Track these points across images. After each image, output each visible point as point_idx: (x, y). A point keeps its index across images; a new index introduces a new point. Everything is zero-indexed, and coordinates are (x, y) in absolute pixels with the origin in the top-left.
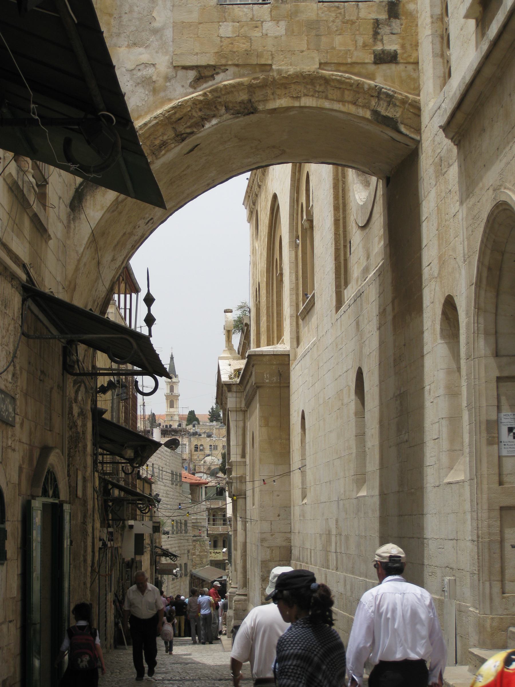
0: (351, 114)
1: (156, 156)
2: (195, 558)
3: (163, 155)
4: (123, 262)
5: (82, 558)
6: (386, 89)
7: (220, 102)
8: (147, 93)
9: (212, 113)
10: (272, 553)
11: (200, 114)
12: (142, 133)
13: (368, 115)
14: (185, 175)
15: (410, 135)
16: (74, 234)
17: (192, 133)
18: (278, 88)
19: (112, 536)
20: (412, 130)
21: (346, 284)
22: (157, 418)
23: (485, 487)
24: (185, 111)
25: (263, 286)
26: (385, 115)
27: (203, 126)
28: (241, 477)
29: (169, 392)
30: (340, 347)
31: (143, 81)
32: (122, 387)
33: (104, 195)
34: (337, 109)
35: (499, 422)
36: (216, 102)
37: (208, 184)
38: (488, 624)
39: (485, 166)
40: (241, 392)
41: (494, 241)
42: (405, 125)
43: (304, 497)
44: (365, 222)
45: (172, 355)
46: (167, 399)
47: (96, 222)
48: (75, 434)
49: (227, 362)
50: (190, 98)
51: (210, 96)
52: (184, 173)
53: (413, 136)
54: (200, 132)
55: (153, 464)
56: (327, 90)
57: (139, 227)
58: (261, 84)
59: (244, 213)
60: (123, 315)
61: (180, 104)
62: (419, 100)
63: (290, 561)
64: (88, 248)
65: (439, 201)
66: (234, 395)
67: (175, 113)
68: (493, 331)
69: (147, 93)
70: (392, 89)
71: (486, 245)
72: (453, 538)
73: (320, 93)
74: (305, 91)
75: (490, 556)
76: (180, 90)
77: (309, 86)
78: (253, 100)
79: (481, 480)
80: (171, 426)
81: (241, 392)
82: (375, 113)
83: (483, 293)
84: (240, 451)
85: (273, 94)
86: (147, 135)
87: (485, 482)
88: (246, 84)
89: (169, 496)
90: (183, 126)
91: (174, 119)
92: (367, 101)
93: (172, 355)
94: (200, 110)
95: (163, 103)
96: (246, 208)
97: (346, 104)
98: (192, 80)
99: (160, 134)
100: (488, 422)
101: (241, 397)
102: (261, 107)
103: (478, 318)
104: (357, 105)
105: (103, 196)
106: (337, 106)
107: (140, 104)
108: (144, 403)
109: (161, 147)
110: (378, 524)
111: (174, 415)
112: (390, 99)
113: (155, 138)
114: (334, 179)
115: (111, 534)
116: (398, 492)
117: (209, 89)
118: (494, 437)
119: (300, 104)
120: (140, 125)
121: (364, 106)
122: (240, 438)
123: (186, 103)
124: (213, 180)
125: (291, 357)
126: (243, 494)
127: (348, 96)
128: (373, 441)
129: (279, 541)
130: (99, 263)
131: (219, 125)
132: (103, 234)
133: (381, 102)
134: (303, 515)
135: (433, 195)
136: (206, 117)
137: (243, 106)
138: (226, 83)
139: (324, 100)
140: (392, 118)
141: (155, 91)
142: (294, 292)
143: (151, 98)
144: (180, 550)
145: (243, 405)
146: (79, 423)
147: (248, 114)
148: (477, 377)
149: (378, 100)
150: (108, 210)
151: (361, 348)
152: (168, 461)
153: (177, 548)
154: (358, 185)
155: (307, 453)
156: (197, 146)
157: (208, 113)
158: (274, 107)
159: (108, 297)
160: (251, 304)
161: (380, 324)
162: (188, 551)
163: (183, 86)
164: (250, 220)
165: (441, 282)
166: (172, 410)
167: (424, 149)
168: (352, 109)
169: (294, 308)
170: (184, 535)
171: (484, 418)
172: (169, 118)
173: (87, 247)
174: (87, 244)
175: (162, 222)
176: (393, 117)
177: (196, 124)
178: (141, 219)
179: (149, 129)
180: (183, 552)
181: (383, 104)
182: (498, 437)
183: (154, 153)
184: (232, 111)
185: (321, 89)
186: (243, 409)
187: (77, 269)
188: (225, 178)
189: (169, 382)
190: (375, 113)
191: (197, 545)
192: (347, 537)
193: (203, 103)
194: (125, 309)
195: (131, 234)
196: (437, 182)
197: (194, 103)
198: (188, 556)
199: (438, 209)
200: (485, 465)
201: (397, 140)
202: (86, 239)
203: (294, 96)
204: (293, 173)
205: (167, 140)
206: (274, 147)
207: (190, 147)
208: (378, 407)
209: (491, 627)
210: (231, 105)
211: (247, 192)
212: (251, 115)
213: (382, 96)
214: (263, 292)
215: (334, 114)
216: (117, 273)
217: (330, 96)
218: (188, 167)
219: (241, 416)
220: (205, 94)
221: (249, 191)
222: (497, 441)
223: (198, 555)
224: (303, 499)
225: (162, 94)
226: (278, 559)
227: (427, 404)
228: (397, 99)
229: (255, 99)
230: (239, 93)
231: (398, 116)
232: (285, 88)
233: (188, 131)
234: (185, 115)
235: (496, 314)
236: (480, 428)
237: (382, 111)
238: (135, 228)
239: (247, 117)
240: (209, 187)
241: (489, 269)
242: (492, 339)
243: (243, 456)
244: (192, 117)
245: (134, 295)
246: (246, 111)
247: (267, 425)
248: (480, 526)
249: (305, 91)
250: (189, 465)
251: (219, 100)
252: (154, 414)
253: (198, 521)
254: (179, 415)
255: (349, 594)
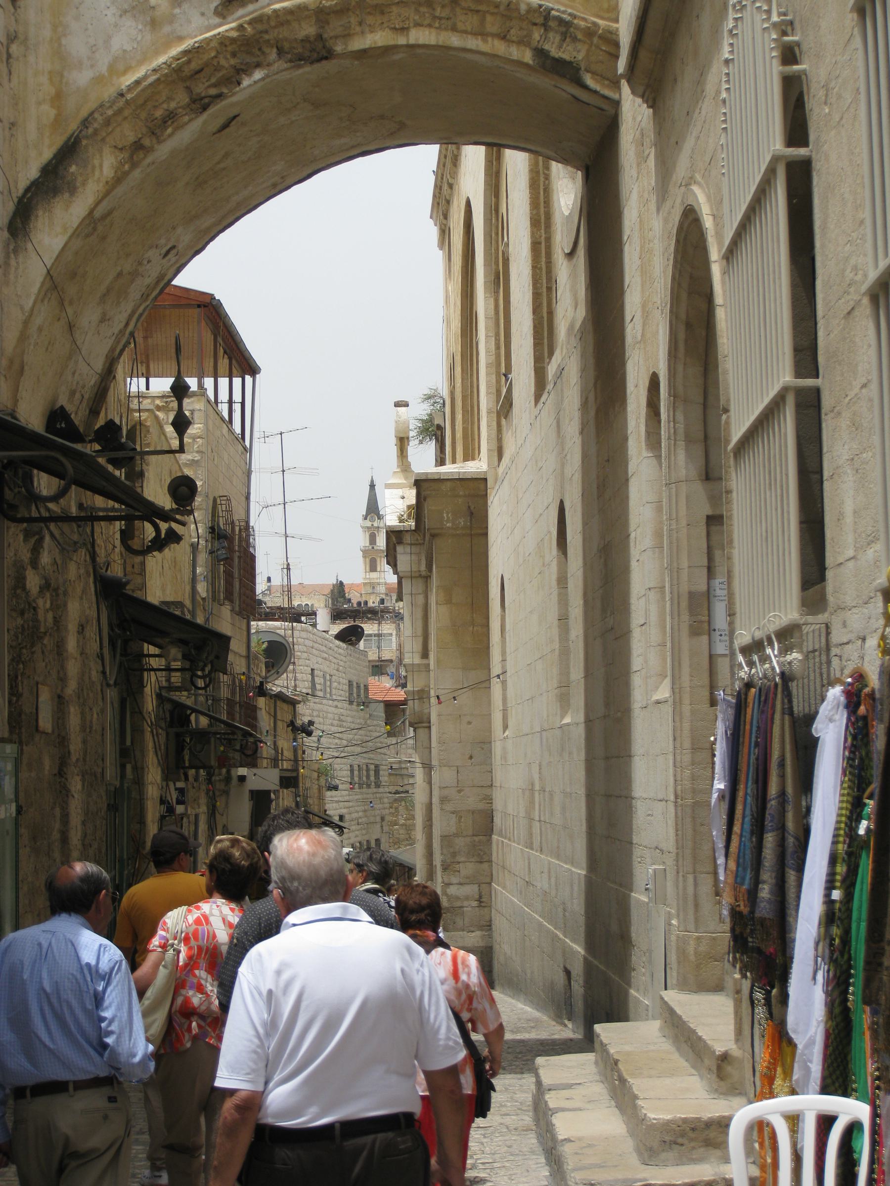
0: (498, 56)
1: (157, 138)
2: (397, 830)
3: (170, 136)
4: (127, 324)
5: (56, 835)
6: (558, 10)
7: (268, 41)
8: (140, 27)
9: (255, 60)
10: (460, 821)
11: (233, 62)
12: (132, 99)
13: (528, 57)
14: (224, 169)
15: (602, 92)
16: (16, 277)
17: (220, 96)
18: (370, 13)
19: (183, 796)
20: (606, 82)
21: (551, 353)
22: (346, 590)
23: (686, 709)
24: (206, 57)
25: (458, 358)
26: (557, 56)
27: (239, 84)
28: (421, 691)
29: (368, 544)
30: (540, 465)
31: (133, 8)
32: (218, 539)
33: (67, 207)
34: (474, 47)
35: (711, 596)
36: (261, 40)
37: (275, 185)
38: (691, 949)
39: (677, 143)
40: (420, 544)
41: (691, 277)
42: (594, 73)
43: (505, 727)
44: (571, 244)
45: (372, 481)
46: (364, 557)
47: (55, 256)
48: (31, 623)
49: (400, 492)
50: (215, 35)
51: (249, 29)
52: (222, 165)
53: (607, 92)
54: (234, 94)
55: (312, 670)
56: (455, 15)
57: (149, 262)
58: (338, 8)
59: (433, 231)
60: (226, 415)
61: (196, 45)
62: (617, 29)
63: (491, 836)
64: (42, 301)
65: (642, 206)
66: (408, 549)
67: (189, 62)
68: (701, 436)
69: (140, 27)
70: (570, 11)
71: (679, 284)
72: (662, 798)
73: (443, 21)
74: (417, 17)
75: (694, 831)
76: (197, 21)
77: (423, 9)
78: (325, 36)
79: (680, 698)
80: (366, 603)
81: (420, 544)
82: (540, 53)
83: (680, 368)
84: (418, 647)
85: (360, 24)
86: (140, 102)
87: (686, 701)
88: (312, 7)
89: (344, 724)
90: (203, 83)
91: (187, 71)
92: (525, 33)
93: (372, 481)
94: (234, 55)
95: (168, 45)
96: (436, 225)
97: (490, 39)
98: (218, 3)
99: (164, 98)
100: (691, 595)
101: (420, 553)
102: (339, 48)
103: (674, 411)
104: (509, 41)
105: (66, 210)
106: (473, 43)
107: (128, 47)
108: (288, 565)
109: (165, 122)
110: (584, 773)
111: (379, 584)
112: (566, 28)
113: (155, 107)
114: (531, 171)
115: (181, 791)
116: (605, 717)
117: (247, 19)
118: (701, 622)
119: (408, 40)
120: (128, 83)
121: (520, 42)
122: (419, 624)
123: (208, 44)
124: (282, 178)
125: (490, 483)
126: (425, 720)
127: (492, 24)
128: (577, 630)
129: (472, 801)
130: (71, 327)
131: (268, 80)
132: (73, 275)
133: (551, 35)
134: (504, 757)
135: (634, 196)
136: (243, 67)
137: (308, 45)
138: (277, 6)
139: (450, 33)
140: (570, 63)
141: (154, 24)
142: (494, 370)
143: (148, 37)
144: (366, 816)
145: (423, 567)
146: (43, 604)
147: (320, 60)
148: (674, 516)
149: (546, 30)
150: (75, 234)
151: (563, 465)
152: (342, 663)
153: (361, 814)
154: (565, 180)
155: (508, 650)
156: (235, 117)
157: (248, 60)
158: (362, 47)
159: (103, 384)
160: (445, 393)
161: (582, 423)
162: (383, 819)
163: (203, 14)
164: (441, 245)
165: (645, 349)
166: (374, 575)
167: (624, 118)
168: (499, 47)
169: (494, 397)
170: (375, 790)
171: (685, 588)
172: (179, 70)
173: (42, 297)
174: (39, 291)
175: (198, 252)
176: (572, 60)
177: (227, 79)
178: (151, 247)
179: (143, 90)
180: (372, 819)
181: (554, 38)
182: (709, 622)
183: (153, 133)
184: (289, 56)
185: (446, 13)
186: (424, 573)
187: (23, 337)
188: (305, 174)
189: (368, 528)
190: (540, 53)
191: (400, 808)
192: (551, 794)
193: (239, 43)
194: (231, 402)
195: (135, 275)
196: (638, 173)
197: (221, 44)
198: (382, 827)
199: (641, 221)
200: (686, 670)
201: (585, 100)
202: (38, 285)
203: (397, 26)
204: (441, 164)
205: (176, 109)
206: (382, 117)
207: (221, 121)
208: (582, 570)
209: (696, 953)
210: (286, 45)
211: (434, 196)
212: (324, 62)
213: (551, 24)
214: (458, 369)
215: (469, 56)
216: (118, 342)
217: (460, 26)
218: (226, 155)
219: (419, 586)
220: (240, 28)
221: (437, 195)
222: (707, 628)
223: (402, 825)
224: (504, 733)
225: (167, 29)
226: (470, 833)
227: (634, 564)
228: (577, 27)
229: (328, 33)
230: (300, 24)
231: (580, 58)
232: (382, 13)
233: (213, 91)
234: (207, 64)
235: (705, 406)
236: (679, 607)
237: (553, 50)
238: (140, 264)
239: (317, 66)
240: (277, 190)
241: (689, 325)
242: (699, 449)
243: (425, 655)
244: (218, 68)
245: (248, 379)
246: (315, 55)
247: (449, 601)
248: (679, 778)
249: (417, 17)
250: (397, 670)
251: (266, 37)
252: (341, 583)
253: (403, 766)
254: (386, 584)
255: (553, 893)
